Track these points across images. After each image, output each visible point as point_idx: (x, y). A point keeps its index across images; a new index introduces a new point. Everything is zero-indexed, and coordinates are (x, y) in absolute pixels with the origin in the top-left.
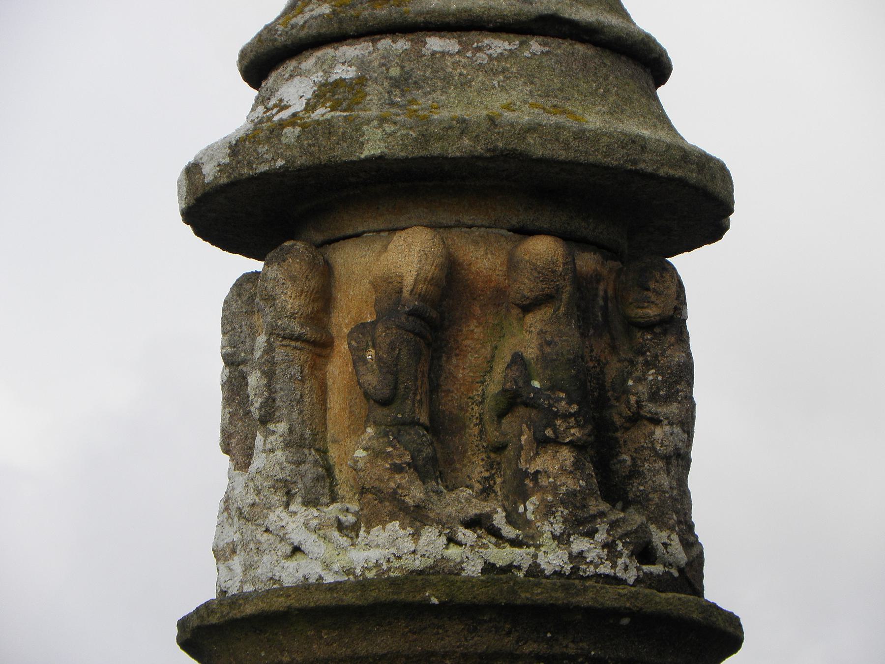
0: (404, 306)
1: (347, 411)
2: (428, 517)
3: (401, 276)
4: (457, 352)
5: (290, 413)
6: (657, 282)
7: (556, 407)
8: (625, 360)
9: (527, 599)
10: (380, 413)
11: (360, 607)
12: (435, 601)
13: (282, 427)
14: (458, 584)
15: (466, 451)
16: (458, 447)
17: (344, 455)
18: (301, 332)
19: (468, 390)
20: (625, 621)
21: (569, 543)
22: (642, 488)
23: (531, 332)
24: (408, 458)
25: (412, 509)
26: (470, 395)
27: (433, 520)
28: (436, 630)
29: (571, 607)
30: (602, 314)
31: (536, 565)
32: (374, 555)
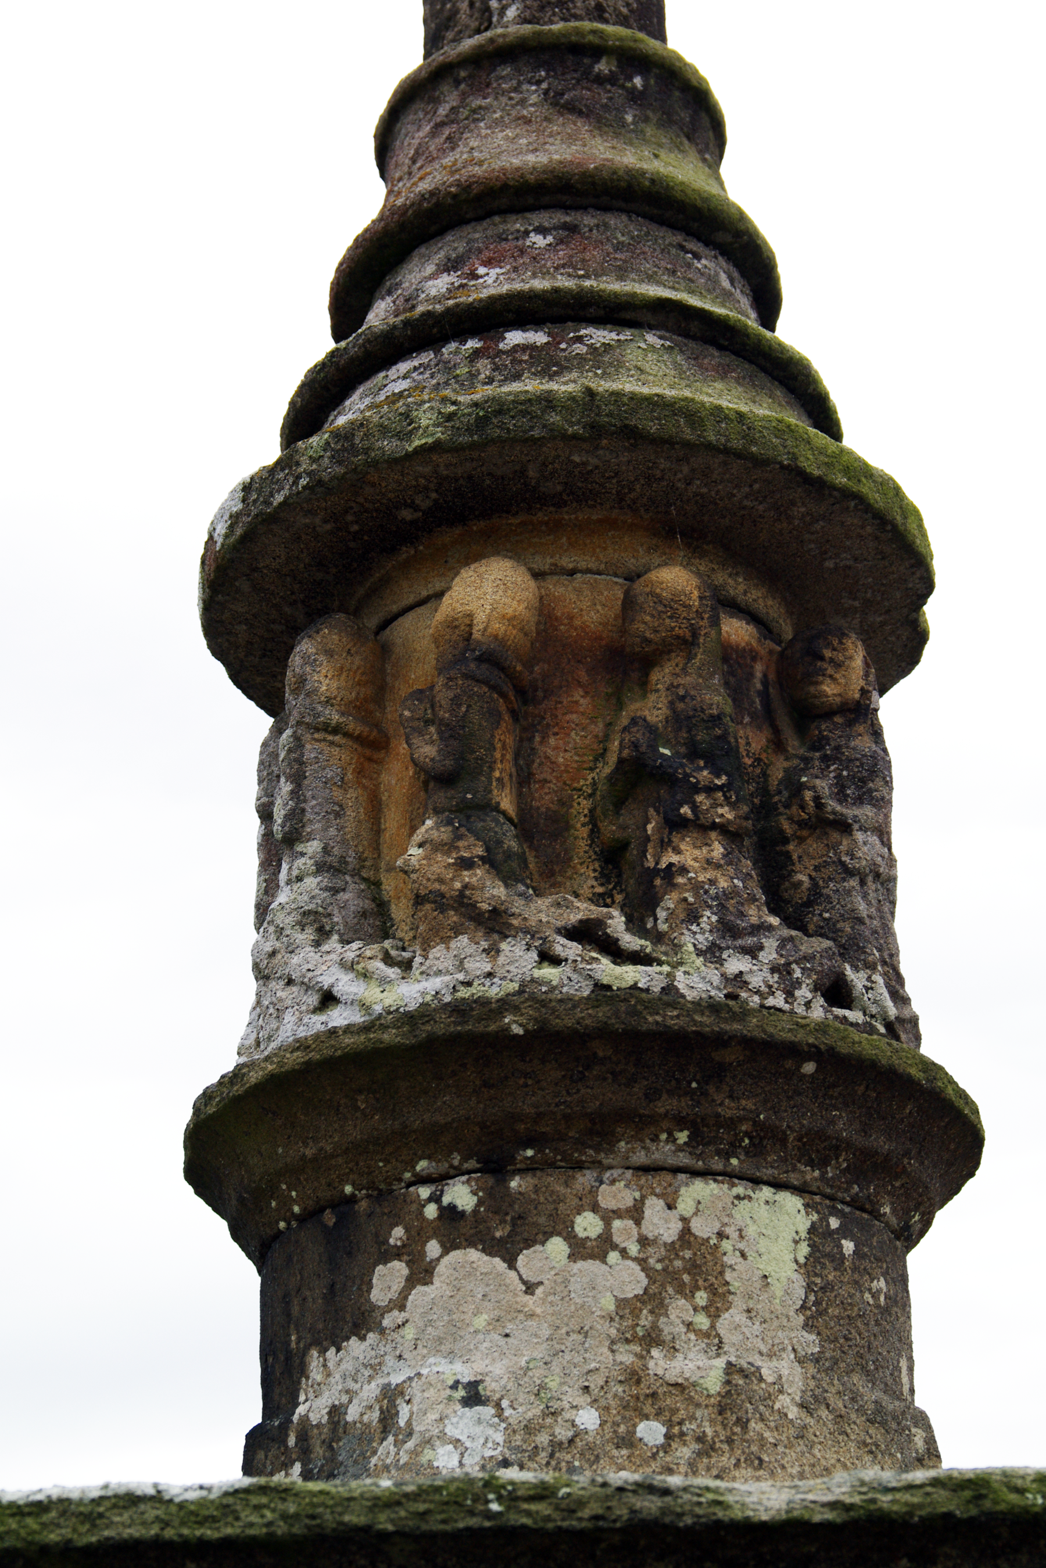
0: (474, 650)
1: (407, 827)
2: (511, 925)
3: (470, 616)
4: (556, 730)
5: (325, 829)
6: (834, 649)
7: (695, 777)
8: (796, 756)
9: (657, 1023)
10: (441, 797)
11: (412, 1048)
12: (517, 1030)
13: (313, 847)
14: (554, 1004)
15: (570, 859)
16: (559, 854)
17: (402, 885)
18: (341, 720)
19: (573, 780)
20: (809, 1068)
21: (721, 962)
22: (827, 915)
23: (657, 691)
24: (480, 851)
25: (487, 915)
26: (576, 785)
27: (518, 929)
28: (523, 1080)
29: (726, 1037)
30: (761, 701)
31: (669, 989)
32: (435, 984)
